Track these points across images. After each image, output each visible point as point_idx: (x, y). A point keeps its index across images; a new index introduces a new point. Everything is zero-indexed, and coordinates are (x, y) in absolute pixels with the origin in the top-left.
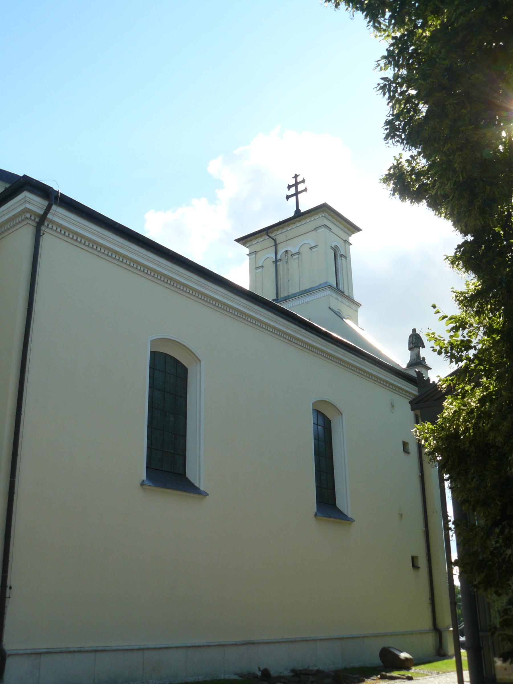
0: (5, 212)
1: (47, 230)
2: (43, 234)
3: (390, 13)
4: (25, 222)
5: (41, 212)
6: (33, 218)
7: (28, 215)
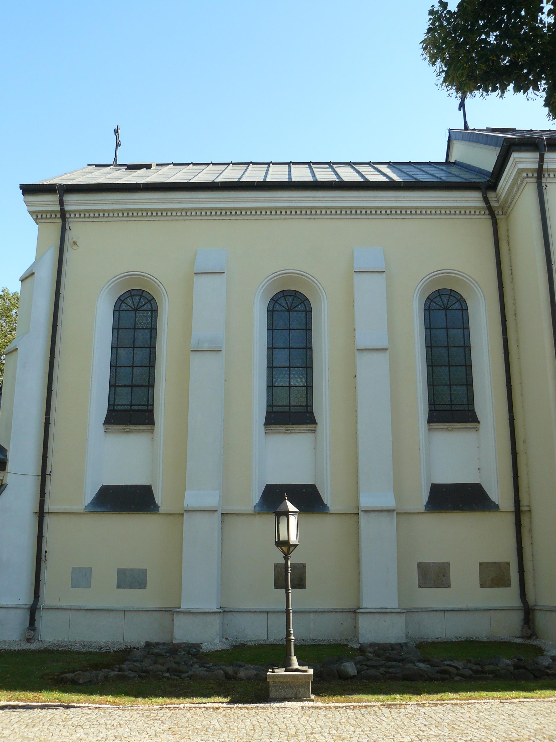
0: (507, 179)
1: (549, 180)
2: (546, 186)
3: (552, 7)
4: (525, 182)
5: (536, 166)
6: (530, 175)
7: (524, 175)
